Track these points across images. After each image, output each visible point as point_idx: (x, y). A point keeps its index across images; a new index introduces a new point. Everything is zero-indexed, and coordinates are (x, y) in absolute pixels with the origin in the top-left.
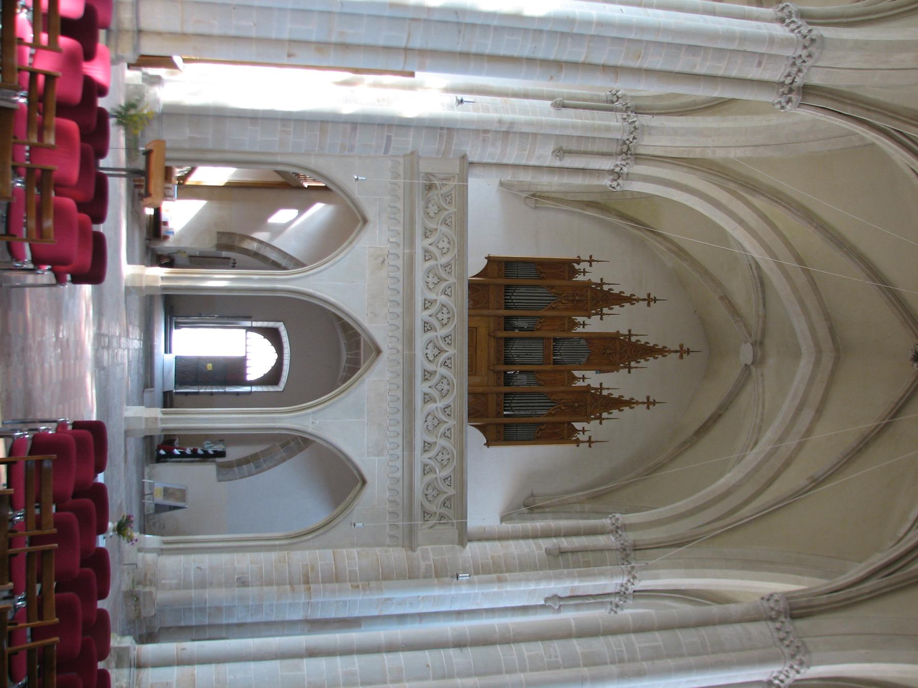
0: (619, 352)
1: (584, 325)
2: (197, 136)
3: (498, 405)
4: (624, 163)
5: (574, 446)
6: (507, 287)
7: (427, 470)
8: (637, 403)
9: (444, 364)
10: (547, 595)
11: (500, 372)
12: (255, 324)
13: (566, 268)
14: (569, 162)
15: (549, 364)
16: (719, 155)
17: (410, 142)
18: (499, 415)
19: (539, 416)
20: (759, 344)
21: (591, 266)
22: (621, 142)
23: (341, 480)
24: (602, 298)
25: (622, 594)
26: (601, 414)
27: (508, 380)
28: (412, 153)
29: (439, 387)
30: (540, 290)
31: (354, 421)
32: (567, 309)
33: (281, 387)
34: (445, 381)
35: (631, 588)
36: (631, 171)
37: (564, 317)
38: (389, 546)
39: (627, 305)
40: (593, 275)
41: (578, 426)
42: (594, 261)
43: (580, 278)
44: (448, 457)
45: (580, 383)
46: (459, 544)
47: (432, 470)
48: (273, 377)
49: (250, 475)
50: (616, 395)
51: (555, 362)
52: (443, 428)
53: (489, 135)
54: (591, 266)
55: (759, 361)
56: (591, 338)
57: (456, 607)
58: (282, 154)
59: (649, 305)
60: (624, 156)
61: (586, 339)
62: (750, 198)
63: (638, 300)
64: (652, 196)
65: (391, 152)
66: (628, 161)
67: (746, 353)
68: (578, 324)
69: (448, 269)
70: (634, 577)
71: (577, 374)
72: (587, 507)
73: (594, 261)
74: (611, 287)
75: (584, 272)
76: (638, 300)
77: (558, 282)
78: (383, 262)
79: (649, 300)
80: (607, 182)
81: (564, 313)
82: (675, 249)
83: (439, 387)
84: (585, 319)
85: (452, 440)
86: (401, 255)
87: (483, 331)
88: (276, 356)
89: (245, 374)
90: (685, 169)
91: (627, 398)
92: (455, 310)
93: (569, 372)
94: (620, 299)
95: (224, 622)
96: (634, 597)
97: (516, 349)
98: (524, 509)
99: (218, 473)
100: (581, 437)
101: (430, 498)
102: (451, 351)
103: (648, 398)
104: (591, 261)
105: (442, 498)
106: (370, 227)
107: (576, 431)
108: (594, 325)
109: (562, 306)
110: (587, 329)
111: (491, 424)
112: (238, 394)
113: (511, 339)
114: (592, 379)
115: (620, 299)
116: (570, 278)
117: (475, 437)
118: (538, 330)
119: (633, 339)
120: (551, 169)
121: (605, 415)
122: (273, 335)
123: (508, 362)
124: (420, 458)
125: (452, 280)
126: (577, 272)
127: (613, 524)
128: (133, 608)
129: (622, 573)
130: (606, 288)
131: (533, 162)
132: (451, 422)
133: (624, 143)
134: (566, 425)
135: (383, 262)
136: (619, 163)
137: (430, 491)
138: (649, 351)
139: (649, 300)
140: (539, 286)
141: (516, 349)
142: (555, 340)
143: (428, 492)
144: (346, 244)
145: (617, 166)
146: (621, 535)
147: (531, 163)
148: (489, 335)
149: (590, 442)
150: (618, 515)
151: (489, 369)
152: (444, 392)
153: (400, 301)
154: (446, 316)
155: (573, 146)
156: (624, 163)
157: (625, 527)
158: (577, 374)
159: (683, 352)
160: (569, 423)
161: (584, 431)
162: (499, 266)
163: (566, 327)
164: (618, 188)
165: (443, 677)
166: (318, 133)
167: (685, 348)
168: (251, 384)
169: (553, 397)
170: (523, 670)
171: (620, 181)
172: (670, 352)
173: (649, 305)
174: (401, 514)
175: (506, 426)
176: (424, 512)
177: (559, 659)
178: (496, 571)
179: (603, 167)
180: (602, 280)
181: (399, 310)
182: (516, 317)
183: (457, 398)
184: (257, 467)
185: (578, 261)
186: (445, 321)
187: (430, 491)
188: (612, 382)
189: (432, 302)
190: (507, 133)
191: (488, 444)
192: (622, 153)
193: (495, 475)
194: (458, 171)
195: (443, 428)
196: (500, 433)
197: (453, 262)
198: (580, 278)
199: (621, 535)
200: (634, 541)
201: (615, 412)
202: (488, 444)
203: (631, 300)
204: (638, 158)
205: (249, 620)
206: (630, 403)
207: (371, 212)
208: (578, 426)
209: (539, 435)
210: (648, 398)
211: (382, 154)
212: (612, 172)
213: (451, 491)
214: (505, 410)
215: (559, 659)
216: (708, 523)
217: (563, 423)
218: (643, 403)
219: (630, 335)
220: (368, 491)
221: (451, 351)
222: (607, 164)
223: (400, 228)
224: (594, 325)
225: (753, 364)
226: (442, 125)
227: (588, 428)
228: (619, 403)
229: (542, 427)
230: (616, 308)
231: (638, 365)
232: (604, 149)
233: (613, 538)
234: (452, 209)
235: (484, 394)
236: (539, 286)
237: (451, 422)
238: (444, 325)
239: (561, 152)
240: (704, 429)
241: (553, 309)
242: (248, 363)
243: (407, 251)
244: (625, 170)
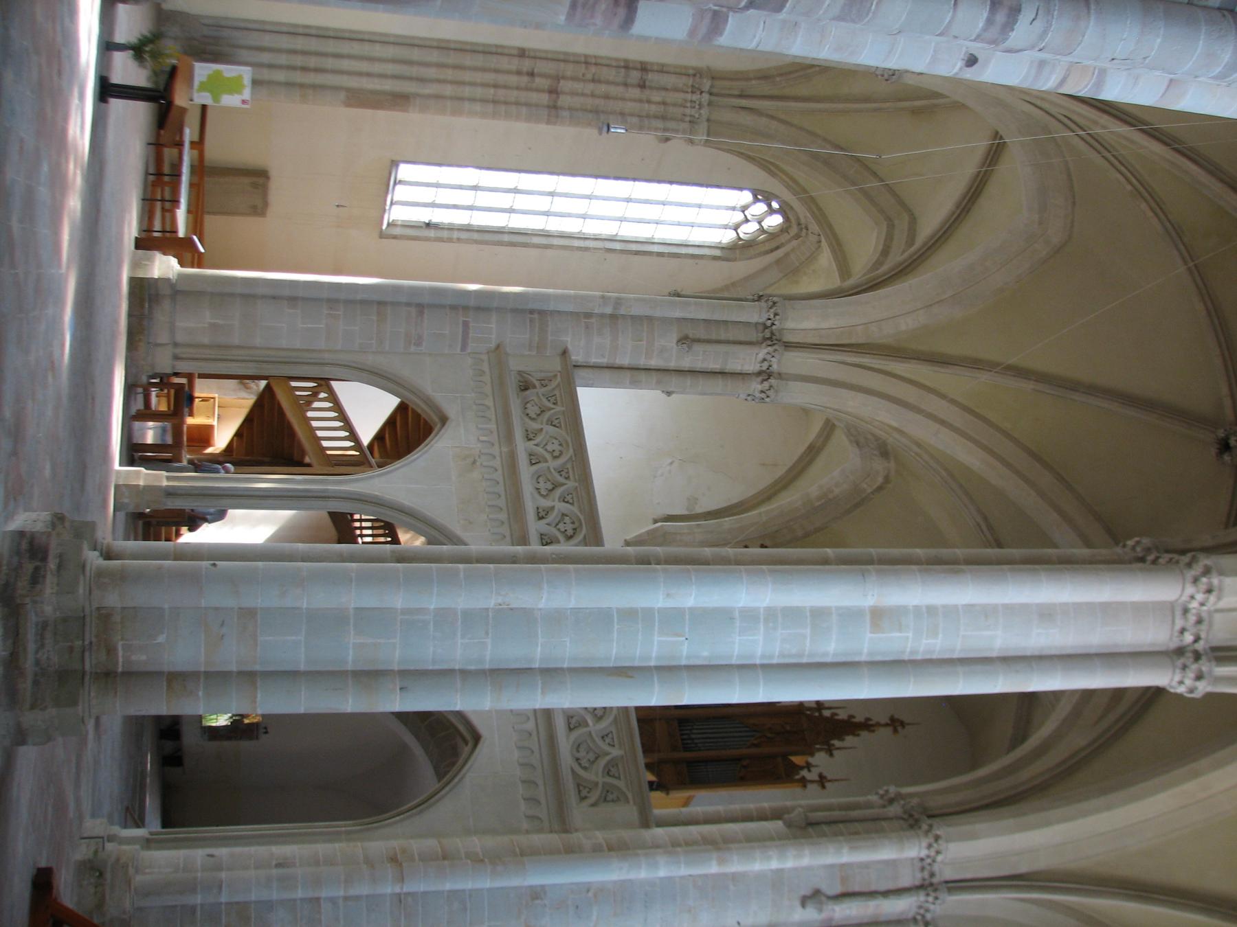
2: (220, 322)
10: (803, 892)
17: (491, 331)
22: (761, 328)
28: (498, 347)
38: (527, 832)
41: (797, 760)
53: (593, 320)
58: (329, 351)
65: (472, 346)
66: (776, 347)
78: (474, 462)
86: (497, 454)
92: (582, 517)
101: (584, 763)
105: (603, 762)
128: (92, 890)
131: (654, 363)
133: (766, 327)
135: (474, 462)
137: (582, 754)
143: (578, 755)
153: (501, 480)
154: (569, 528)
155: (701, 333)
166: (375, 318)
171: (772, 381)
174: (540, 782)
176: (578, 785)
181: (503, 516)
186: (570, 532)
187: (582, 754)
189: (548, 511)
190: (613, 317)
192: (765, 339)
194: (559, 368)
197: (569, 466)
207: (451, 410)
208: (797, 760)
211: (458, 351)
220: (483, 749)
223: (493, 426)
226: (531, 306)
234: (571, 484)
238: (555, 457)
243: (505, 449)
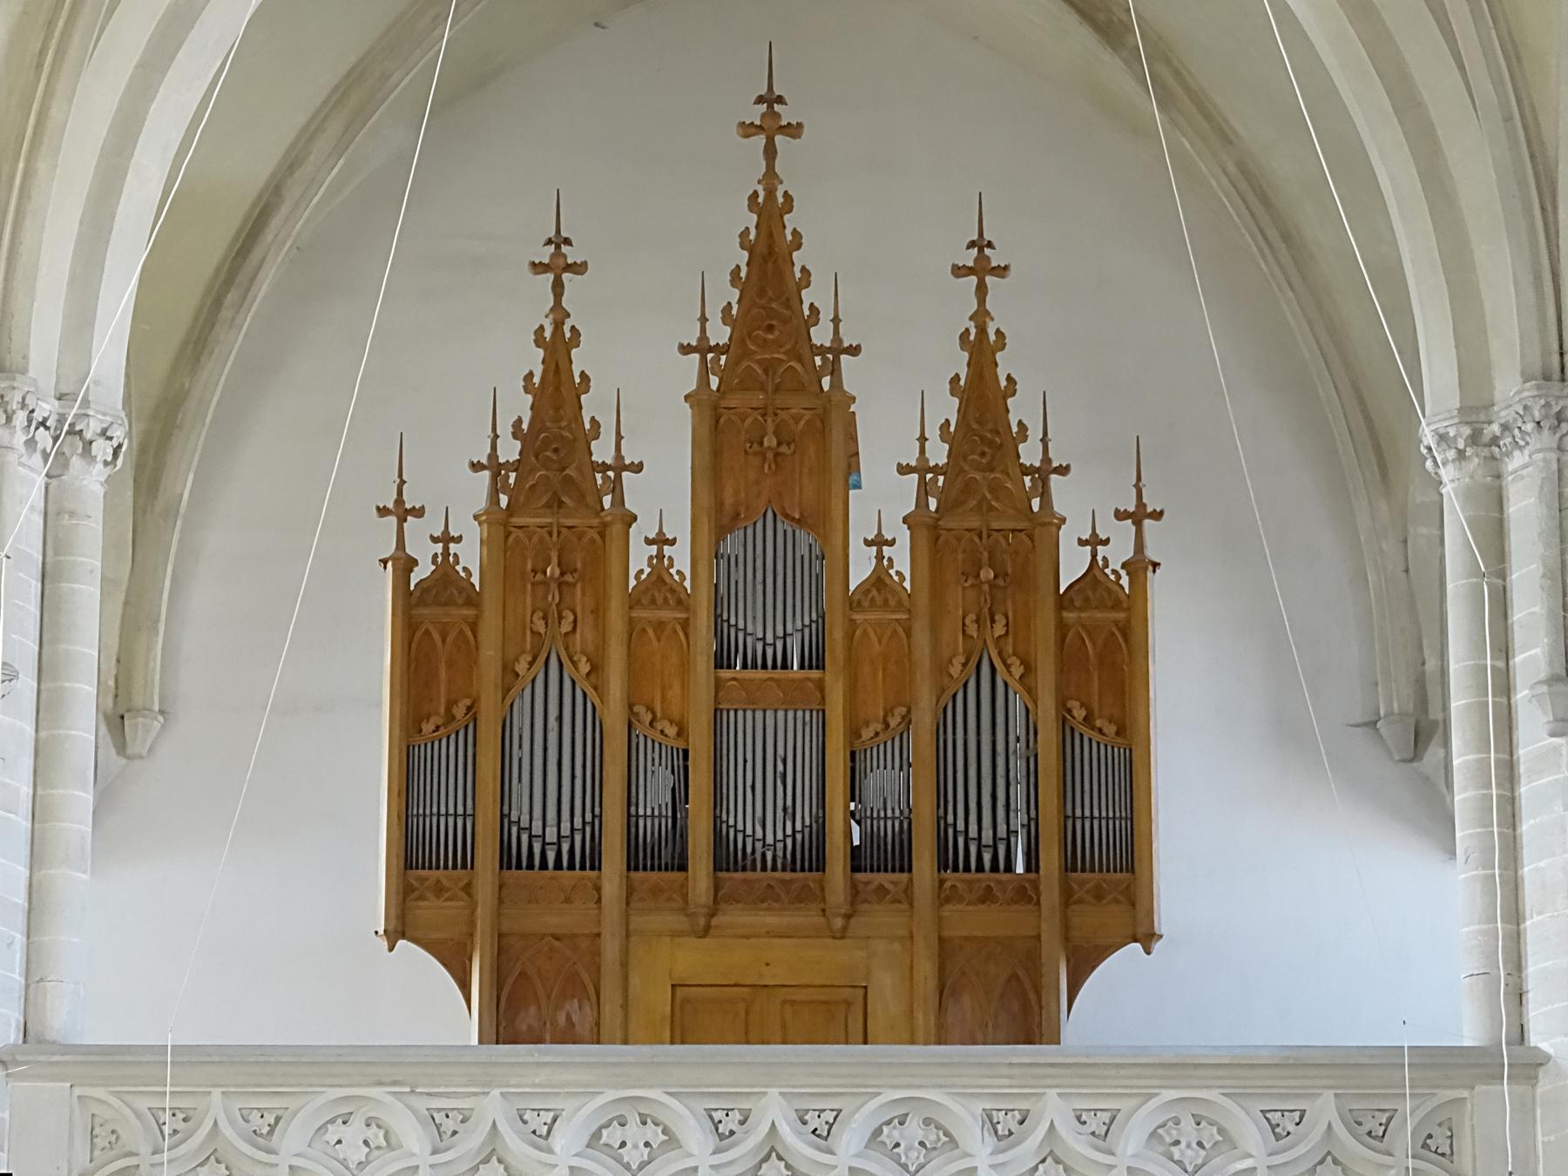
0: (771, 391)
1: (661, 540)
3: (987, 896)
4: (20, 418)
5: (1156, 584)
6: (508, 859)
8: (981, 316)
9: (822, 1136)
11: (855, 891)
13: (432, 619)
15: (820, 686)
18: (1027, 894)
19: (1032, 730)
21: (419, 512)
24: (554, 465)
26: (1026, 470)
27: (883, 855)
30: (521, 722)
32: (599, 612)
34: (890, 1135)
36: (48, 384)
37: (631, 622)
39: (580, 361)
40: (458, 505)
41: (1072, 565)
42: (399, 501)
43: (470, 557)
44: (1188, 1124)
45: (901, 559)
46: (1532, 1080)
50: (947, 409)
51: (815, 659)
52: (1076, 1143)
54: (419, 512)
56: (719, 516)
59: (579, 268)
61: (721, 532)
63: (559, 314)
68: (660, 564)
69: (449, 1125)
71: (860, 569)
73: (399, 501)
74: (505, 429)
76: (559, 314)
77: (490, 652)
79: (558, 266)
82: (334, 128)
83: (915, 1157)
84: (637, 535)
85: (1124, 1105)
87: (693, 959)
90: (42, 166)
91: (960, 364)
92: (612, 1095)
93: (853, 603)
94: (557, 390)
100: (1117, 553)
102: (774, 1110)
104: (403, 512)
109: (585, 635)
110: (680, 527)
111: (1066, 927)
113: (719, 839)
114: (880, 510)
115: (557, 390)
116: (473, 599)
117: (1114, 1001)
118: (682, 733)
119: (720, 334)
121: (1030, 454)
123: (810, 855)
125: (493, 1108)
126: (445, 568)
127: (1461, 454)
130: (510, 451)
132: (1054, 1109)
134: (1070, 616)
136: (20, 438)
138: (769, 271)
139: (558, 266)
140: (505, 727)
141: (763, 822)
142: (722, 661)
145: (31, 443)
146: (1505, 427)
147: (26, 790)
148: (706, 932)
149: (1138, 516)
151: (843, 935)
152: (931, 1137)
156: (20, 418)
157: (1475, 410)
158: (860, 569)
159: (771, 124)
160: (1063, 602)
161: (1095, 541)
162: (431, 877)
163: (665, 615)
164: (119, 433)
167: (756, 114)
169: (956, 669)
171: (91, 428)
173: (579, 268)
175: (1070, 864)
179: (36, 495)
180: (476, 467)
182: (631, 820)
183: (960, 1089)
186: (657, 1137)
188: (896, 422)
191: (1148, 938)
195: (1076, 1143)
196: (1101, 881)
197: (422, 1104)
198: (470, 557)
199: (1505, 427)
200: (1526, 378)
201: (1019, 410)
202: (1148, 938)
206: (982, 348)
208: (1072, 565)
209: (1111, 729)
213: (1324, 1109)
214: (1009, 868)
217: (1062, 628)
221: (774, 1110)
227: (1083, 520)
229: (1079, 713)
230: (592, 406)
231: (826, 316)
233: (1517, 461)
234: (216, 1107)
235: (945, 949)
236: (505, 727)
237: (1054, 1109)
241: (596, 668)
244: (46, 408)
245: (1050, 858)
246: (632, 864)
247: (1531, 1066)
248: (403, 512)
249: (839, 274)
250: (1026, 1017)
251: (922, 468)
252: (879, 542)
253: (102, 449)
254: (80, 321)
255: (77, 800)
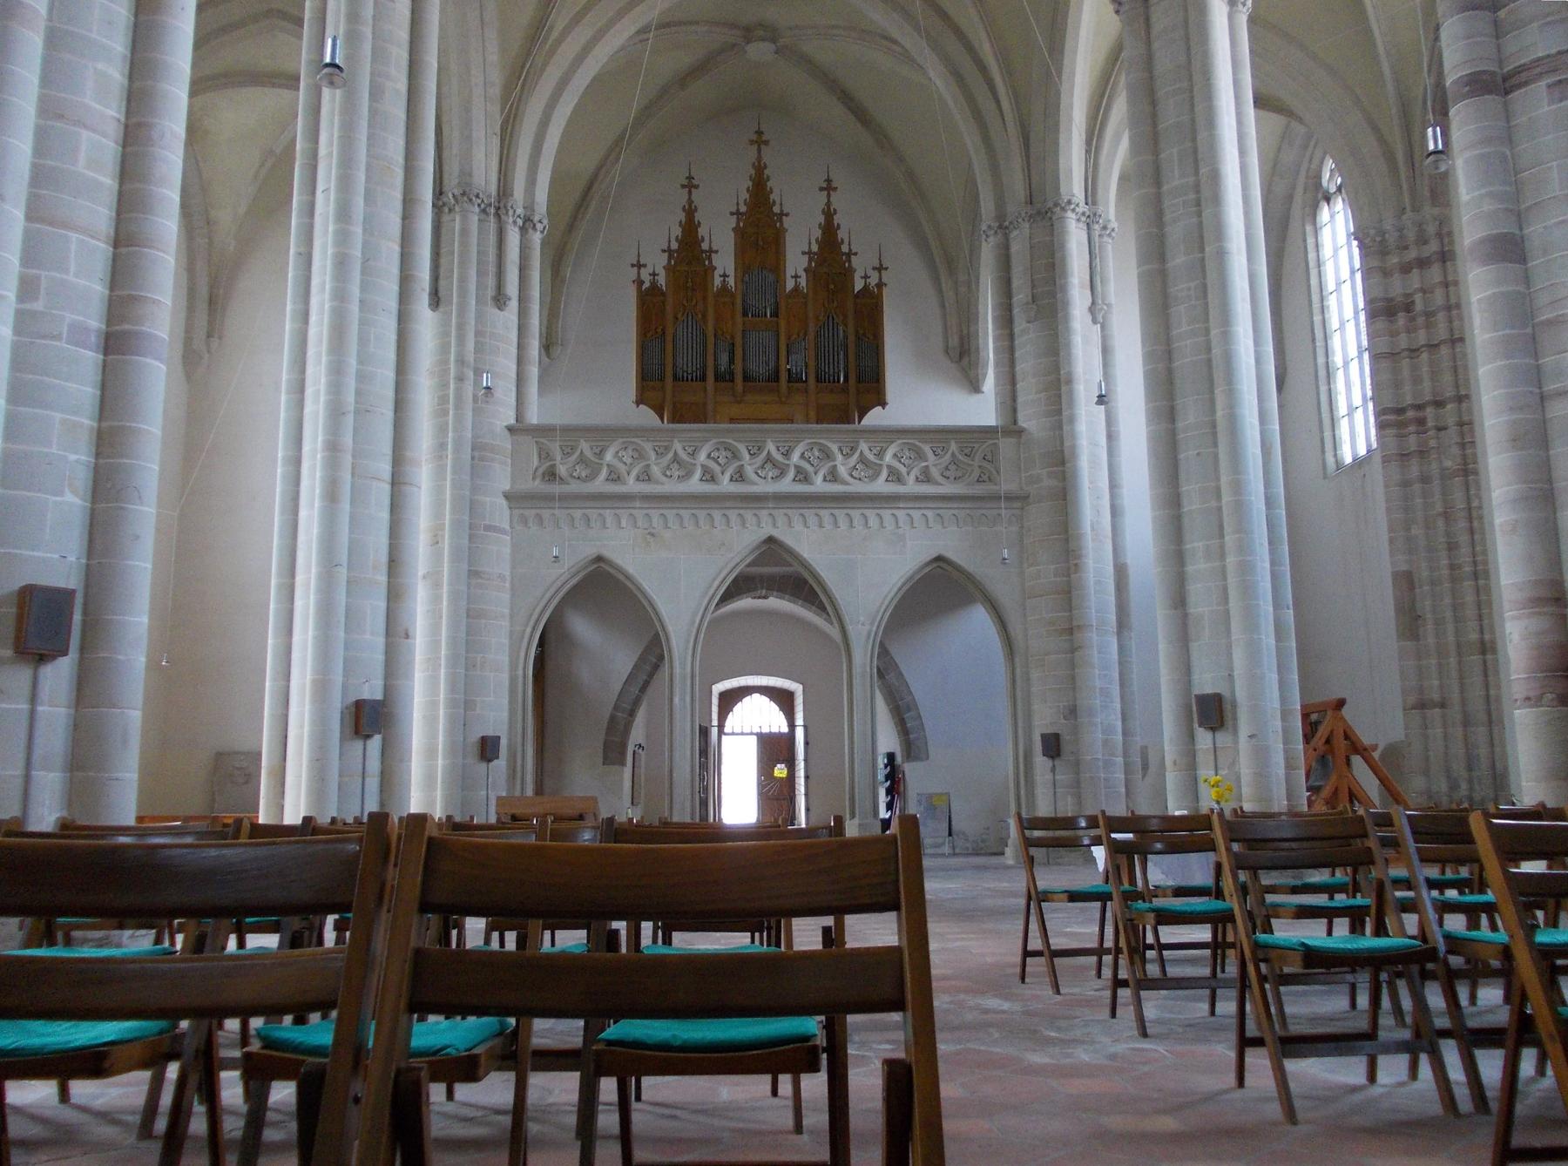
0: (760, 229)
1: (725, 276)
3: (832, 391)
5: (885, 291)
6: (675, 378)
7: (926, 477)
8: (828, 204)
12: (715, 723)
13: (649, 299)
14: (512, 289)
16: (496, 77)
18: (845, 390)
19: (846, 337)
20: (749, 33)
23: (938, 590)
24: (689, 252)
25: (1090, 221)
29: (816, 462)
31: (867, 561)
32: (705, 298)
33: (796, 688)
35: (1082, 208)
40: (657, 263)
41: (859, 285)
43: (662, 280)
45: (803, 282)
47: (926, 471)
48: (784, 699)
49: (920, 717)
50: (818, 233)
55: (771, 33)
56: (744, 267)
57: (1103, 441)
60: (502, 211)
62: (555, 34)
63: (690, 202)
64: (555, 171)
67: (759, 51)
70: (1069, 202)
72: (962, 277)
75: (654, 274)
76: (690, 202)
77: (669, 308)
79: (690, 185)
80: (536, 238)
81: (711, 300)
84: (717, 274)
88: (756, 696)
89: (780, 735)
91: (822, 219)
94: (690, 227)
95: (1120, 738)
96: (1094, 203)
97: (759, 368)
98: (966, 360)
99: (917, 758)
100: (873, 281)
103: (821, 189)
104: (639, 266)
106: (607, 553)
107: (866, 287)
108: (725, 263)
110: (731, 271)
112: (807, 743)
114: (796, 264)
115: (690, 227)
116: (663, 294)
117: (875, 417)
119: (743, 209)
120: (523, 313)
121: (845, 249)
122: (730, 700)
123: (775, 377)
124: (911, 487)
126: (654, 285)
129: (1062, 219)
130: (675, 246)
135: (653, 535)
138: (760, 188)
139: (690, 185)
141: (759, 368)
144: (628, 584)
147: (515, 339)
150: (984, 228)
155: (491, 281)
157: (1001, 216)
159: (760, 141)
160: (857, 296)
161: (866, 277)
164: (545, 222)
165: (1215, 434)
167: (755, 137)
168: (792, 726)
170: (1207, 331)
171: (536, 219)
172: (759, 158)
177: (1192, 285)
178: (1057, 386)
182: (716, 367)
183: (832, 438)
184: (909, 710)
185: (640, 282)
186: (729, 455)
191: (883, 404)
193: (917, 397)
196: (871, 389)
198: (662, 280)
201: (841, 234)
202: (883, 404)
203: (690, 211)
204: (504, 191)
205: (1118, 706)
206: (829, 214)
207: (590, 551)
208: (859, 285)
210: (821, 189)
212: (523, 230)
213: (953, 447)
215: (1192, 285)
216: (998, 102)
218: (829, 196)
219: (738, 213)
220: (950, 555)
222: (513, 238)
224: (725, 263)
225: (774, 41)
228: (829, 230)
232: (492, 239)
233: (1015, 233)
239: (500, 300)
240: (861, 115)
241: (704, 316)
242: (765, 730)
245: (852, 381)
246: (716, 379)
247: (1020, 432)
248: (639, 266)
249: (782, 192)
250: (845, 418)
251: (809, 253)
252: (796, 277)
253: (540, 227)
254: (531, 181)
255: (534, 371)
